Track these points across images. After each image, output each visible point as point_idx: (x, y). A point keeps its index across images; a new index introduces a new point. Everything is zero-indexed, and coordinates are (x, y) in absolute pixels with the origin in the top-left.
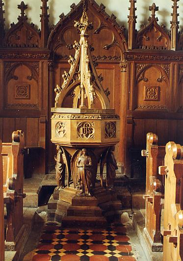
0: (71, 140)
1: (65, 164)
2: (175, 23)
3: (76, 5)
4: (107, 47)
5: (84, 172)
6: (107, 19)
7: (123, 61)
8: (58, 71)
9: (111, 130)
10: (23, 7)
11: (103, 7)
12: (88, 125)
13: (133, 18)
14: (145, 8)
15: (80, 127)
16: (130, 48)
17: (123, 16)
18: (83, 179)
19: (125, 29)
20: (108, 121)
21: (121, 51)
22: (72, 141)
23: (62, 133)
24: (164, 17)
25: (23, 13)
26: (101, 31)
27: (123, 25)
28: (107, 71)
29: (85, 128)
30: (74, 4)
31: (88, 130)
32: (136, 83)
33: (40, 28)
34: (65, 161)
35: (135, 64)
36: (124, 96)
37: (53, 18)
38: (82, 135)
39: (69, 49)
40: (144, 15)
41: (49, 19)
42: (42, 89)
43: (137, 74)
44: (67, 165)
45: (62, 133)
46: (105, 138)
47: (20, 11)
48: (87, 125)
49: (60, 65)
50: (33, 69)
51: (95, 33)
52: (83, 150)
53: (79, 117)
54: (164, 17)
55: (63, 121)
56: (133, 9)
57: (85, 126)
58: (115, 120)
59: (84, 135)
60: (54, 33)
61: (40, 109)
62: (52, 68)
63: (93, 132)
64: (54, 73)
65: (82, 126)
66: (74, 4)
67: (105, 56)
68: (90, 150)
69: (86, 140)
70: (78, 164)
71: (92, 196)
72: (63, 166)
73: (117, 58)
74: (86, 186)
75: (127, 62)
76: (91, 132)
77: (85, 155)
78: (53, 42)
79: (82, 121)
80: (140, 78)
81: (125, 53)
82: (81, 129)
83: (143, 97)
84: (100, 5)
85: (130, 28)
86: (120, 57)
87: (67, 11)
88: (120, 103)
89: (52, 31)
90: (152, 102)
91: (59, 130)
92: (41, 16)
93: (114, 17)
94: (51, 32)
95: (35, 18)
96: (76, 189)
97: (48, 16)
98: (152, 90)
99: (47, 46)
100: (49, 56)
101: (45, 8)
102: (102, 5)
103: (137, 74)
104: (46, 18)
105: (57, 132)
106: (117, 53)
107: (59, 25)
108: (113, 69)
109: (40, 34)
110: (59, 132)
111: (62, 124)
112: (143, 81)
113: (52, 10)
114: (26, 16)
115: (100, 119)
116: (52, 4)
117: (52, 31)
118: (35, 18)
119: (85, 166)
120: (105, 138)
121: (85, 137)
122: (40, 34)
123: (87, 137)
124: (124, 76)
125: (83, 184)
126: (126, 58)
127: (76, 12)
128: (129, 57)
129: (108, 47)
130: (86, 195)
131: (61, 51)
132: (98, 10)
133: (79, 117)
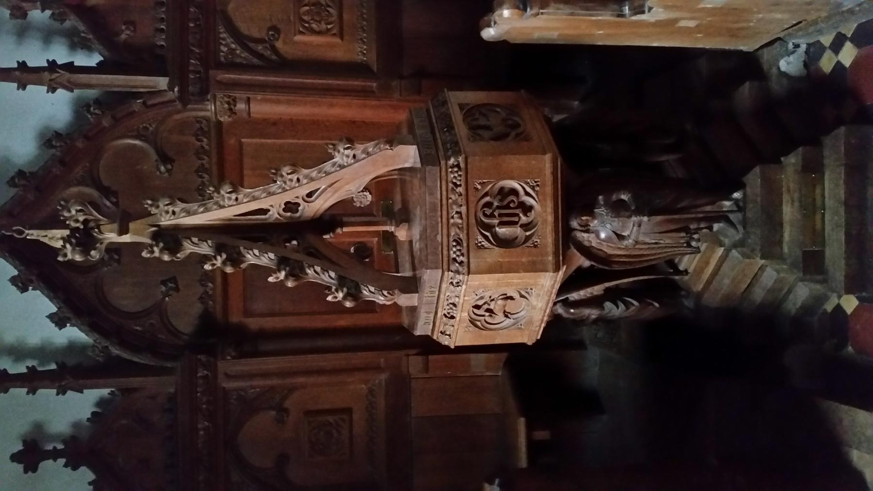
0: (547, 271)
1: (607, 290)
2: (54, 76)
3: (16, 273)
4: (165, 164)
5: (659, 218)
6: (62, 162)
7: (210, 109)
8: (253, 323)
9: (494, 121)
10: (31, 454)
11: (21, 177)
12: (488, 205)
13: (53, 75)
14: (22, 33)
15: (495, 235)
16: (162, 82)
17: (55, 107)
18: (679, 220)
19: (97, 102)
20: (462, 130)
21: (177, 117)
22: (550, 266)
23: (510, 306)
24: (39, 30)
25: (55, 455)
26: (106, 183)
27: (81, 108)
28: (247, 161)
29: (500, 215)
30: (14, 281)
31: (507, 207)
32: (284, 65)
33: (105, 392)
34: (597, 290)
35: (220, 66)
36: (331, 105)
37: (72, 347)
38: (526, 227)
39: (177, 289)
40: (48, 37)
41: (71, 362)
42: (320, 372)
43: (255, 61)
44: (607, 285)
45: (510, 306)
46: (527, 139)
47: (47, 465)
48: (488, 211)
49: (235, 318)
50: (250, 406)
51: (116, 204)
52: (575, 224)
53: (459, 242)
54: (39, 30)
55: (472, 300)
56: (23, 75)
57: (492, 216)
58: (457, 108)
59: (524, 219)
60: (123, 344)
61: (383, 377)
62: (247, 343)
63: (515, 185)
64: (263, 335)
65: (489, 228)
66: (14, 281)
67: (197, 171)
68: (574, 202)
69: (543, 211)
70: (625, 243)
71: (740, 186)
72: (612, 295)
73: (202, 128)
74: (708, 208)
75: (215, 97)
76: (514, 192)
77: (592, 214)
78: (152, 347)
79: (475, 229)
80: (268, 53)
81: (184, 98)
82: (502, 231)
83: (332, 46)
84: (13, 191)
85: (94, 82)
86: (198, 120)
87: (40, 304)
88: (354, 122)
89: (115, 351)
90: (346, 16)
91: (500, 317)
92: (62, 391)
93: (50, 139)
94: (118, 357)
95: (71, 409)
96: (703, 247)
97: (62, 366)
98: (307, 13)
99: (169, 365)
100: (203, 358)
101: (32, 380)
102: (12, 183)
103: (255, 61)
104: (67, 372)
105: (508, 322)
106: (182, 128)
107: (92, 326)
108: (241, 144)
109: (126, 391)
110: (506, 315)
111: (478, 307)
112: (279, 45)
113: (42, 352)
114: (64, 442)
115: (461, 159)
116: (17, 352)
117: (115, 351)
118: (71, 409)
119: (639, 212)
120: (527, 139)
121: (532, 215)
122: (126, 391)
123: (531, 208)
124: (263, 108)
125: (699, 220)
126: (203, 95)
127: (37, 269)
128: (193, 89)
129: (165, 158)
130: (740, 207)
131: (185, 321)
132: (31, 197)
133: (459, 242)
